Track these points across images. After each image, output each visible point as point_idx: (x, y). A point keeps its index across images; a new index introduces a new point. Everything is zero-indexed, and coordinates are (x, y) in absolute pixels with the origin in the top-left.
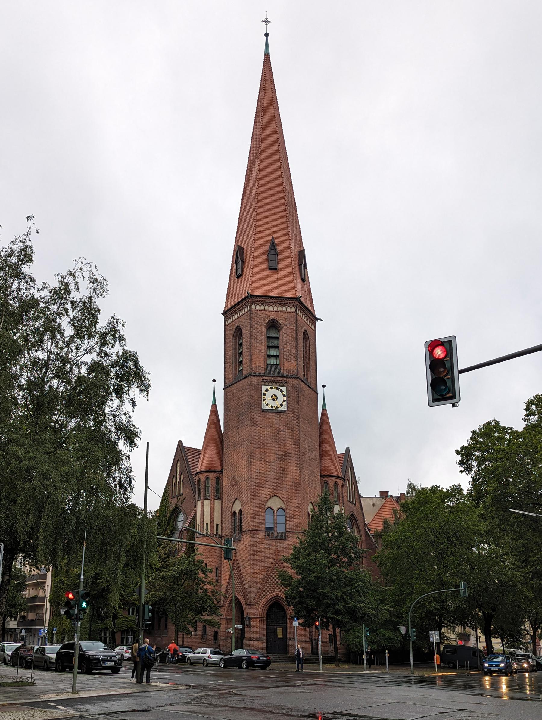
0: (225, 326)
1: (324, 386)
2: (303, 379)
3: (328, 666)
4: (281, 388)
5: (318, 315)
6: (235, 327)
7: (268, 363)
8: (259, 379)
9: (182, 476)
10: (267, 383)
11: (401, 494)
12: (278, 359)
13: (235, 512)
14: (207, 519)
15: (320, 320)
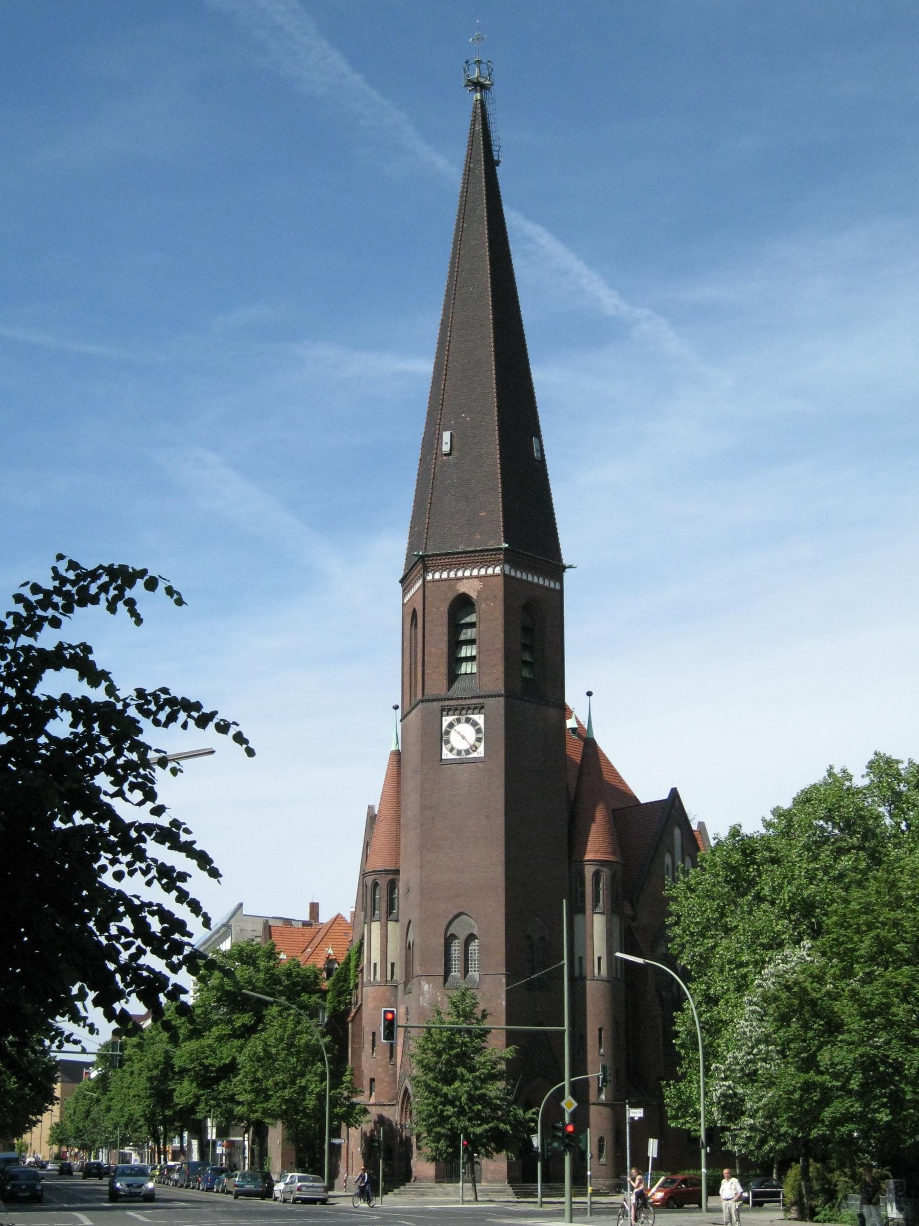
0: (404, 605)
5: (566, 561)
8: (436, 705)
14: (376, 957)
15: (570, 567)
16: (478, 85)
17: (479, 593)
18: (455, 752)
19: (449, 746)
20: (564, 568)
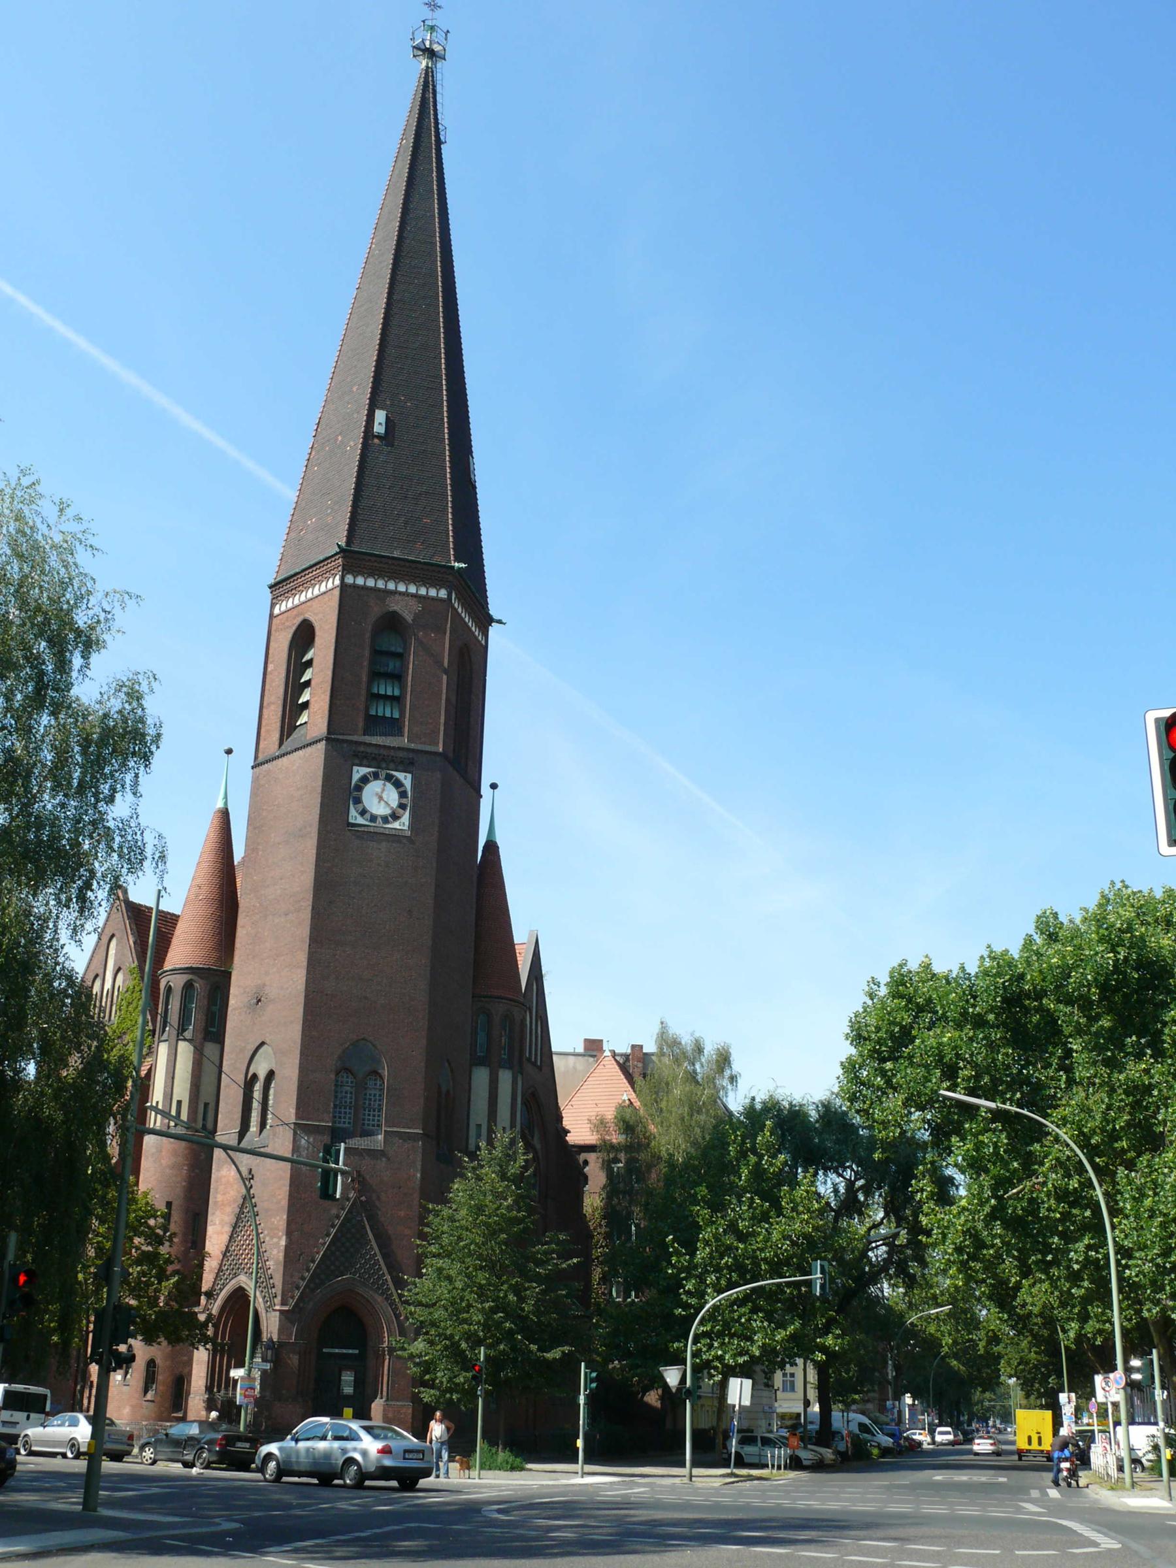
1: (494, 786)
2: (453, 767)
3: (373, 1414)
4: (400, 775)
5: (494, 610)
6: (300, 619)
7: (373, 712)
9: (120, 976)
10: (365, 762)
11: (633, 1047)
12: (395, 704)
13: (255, 1076)
15: (499, 622)
16: (430, 53)
17: (417, 617)
18: (368, 816)
19: (360, 807)
20: (490, 620)
